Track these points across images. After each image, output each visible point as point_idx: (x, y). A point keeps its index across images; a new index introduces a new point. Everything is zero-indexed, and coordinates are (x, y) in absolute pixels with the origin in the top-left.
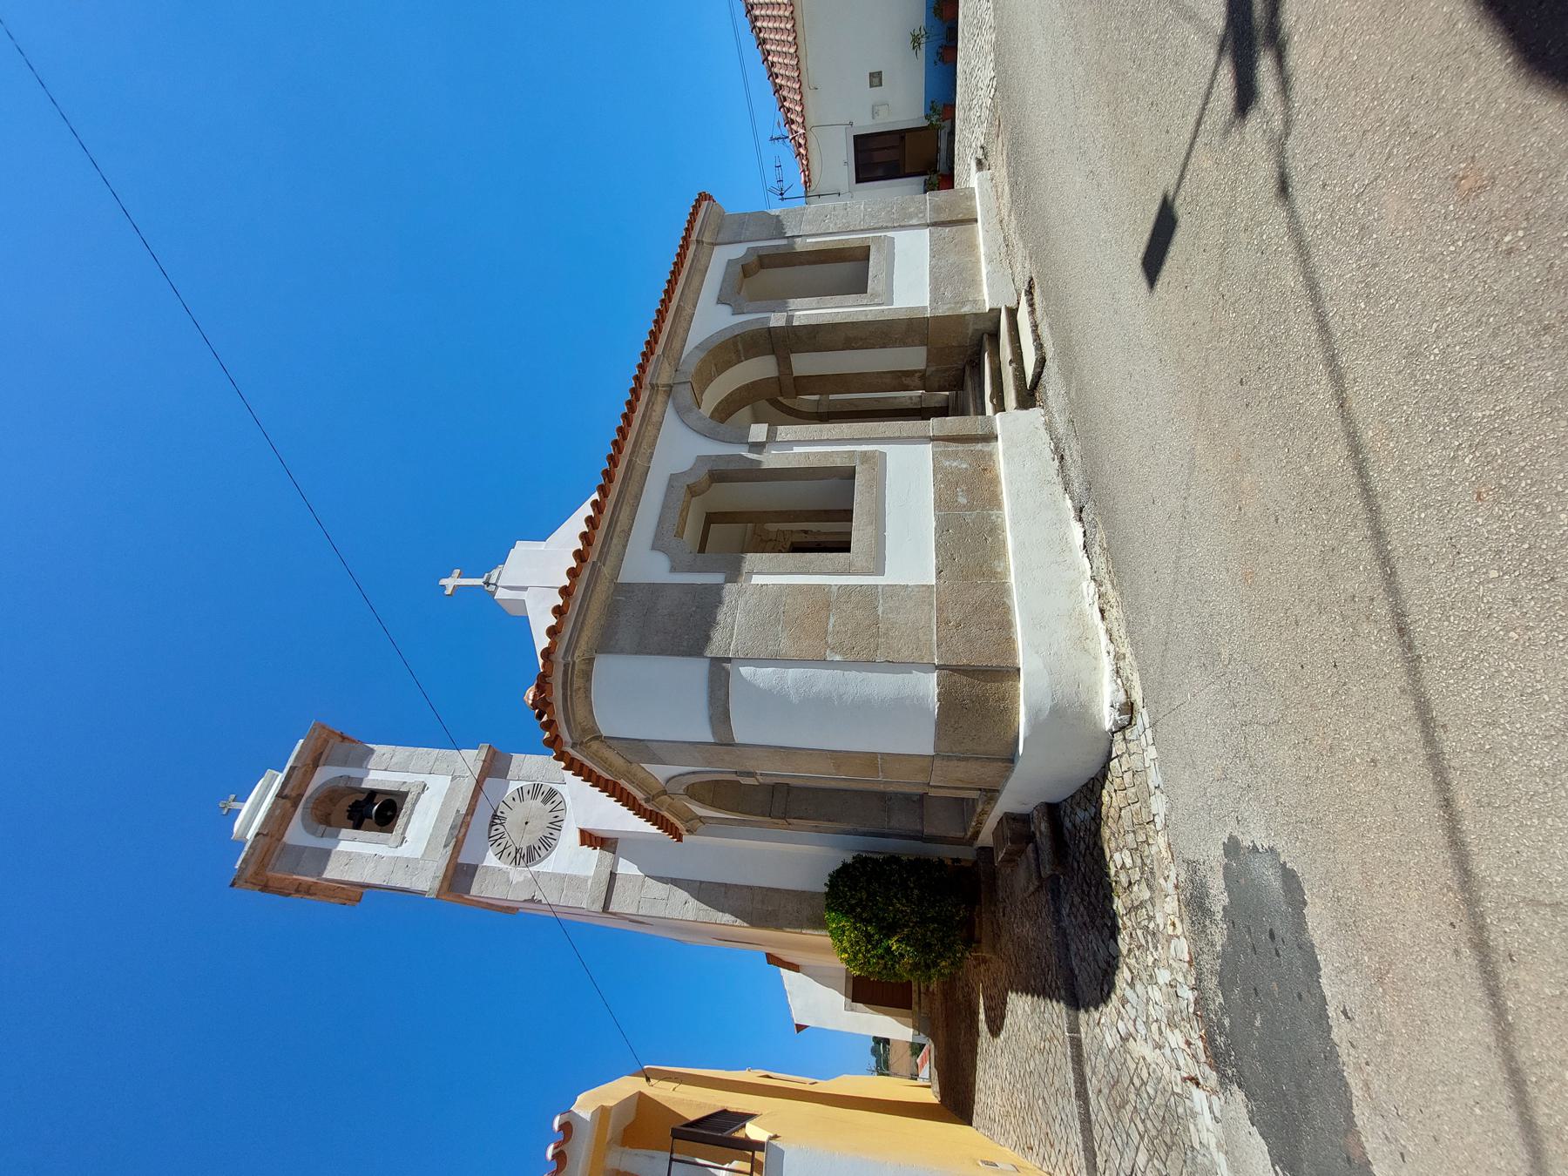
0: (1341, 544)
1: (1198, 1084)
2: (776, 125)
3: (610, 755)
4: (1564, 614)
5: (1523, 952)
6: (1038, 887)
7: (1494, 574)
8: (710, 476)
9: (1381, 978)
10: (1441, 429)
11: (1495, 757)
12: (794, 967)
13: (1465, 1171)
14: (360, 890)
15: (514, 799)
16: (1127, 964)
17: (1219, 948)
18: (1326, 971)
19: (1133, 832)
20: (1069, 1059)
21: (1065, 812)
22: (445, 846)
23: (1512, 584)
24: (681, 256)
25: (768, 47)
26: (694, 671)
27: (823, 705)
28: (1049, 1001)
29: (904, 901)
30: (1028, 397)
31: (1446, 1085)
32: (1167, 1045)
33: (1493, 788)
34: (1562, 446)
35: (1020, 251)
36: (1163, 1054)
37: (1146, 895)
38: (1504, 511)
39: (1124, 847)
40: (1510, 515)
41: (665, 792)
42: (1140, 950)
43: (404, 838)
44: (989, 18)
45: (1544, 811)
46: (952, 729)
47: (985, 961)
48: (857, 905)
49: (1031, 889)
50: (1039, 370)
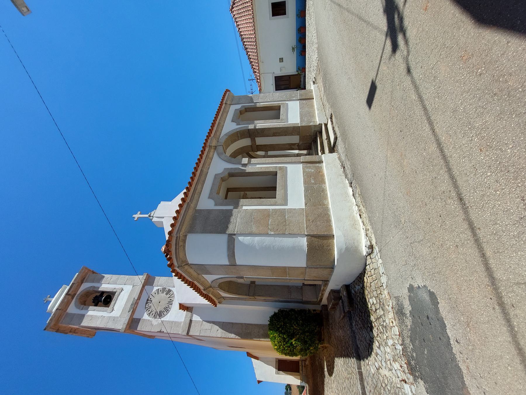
0: (438, 175)
1: (406, 382)
2: (250, 75)
3: (191, 271)
4: (514, 182)
5: (517, 303)
6: (344, 316)
7: (489, 174)
8: (228, 175)
9: (468, 325)
10: (466, 132)
11: (498, 235)
12: (256, 358)
13: (508, 394)
14: (94, 331)
15: (155, 293)
16: (377, 340)
17: (409, 327)
18: (448, 326)
19: (376, 290)
20: (358, 380)
21: (352, 288)
22: (129, 312)
23: (495, 176)
24: (220, 107)
25: (248, 50)
26: (222, 239)
27: (267, 250)
28: (350, 359)
29: (297, 325)
30: (332, 150)
31: (497, 360)
32: (393, 369)
33: (498, 246)
34: (505, 129)
35: (328, 106)
36: (392, 373)
37: (382, 313)
38: (490, 153)
39: (373, 297)
40: (492, 154)
41: (211, 287)
42: (381, 334)
43: (113, 309)
44: (315, 41)
45: (517, 250)
46: (312, 257)
47: (326, 348)
48: (280, 327)
49: (342, 316)
50: (335, 141)
